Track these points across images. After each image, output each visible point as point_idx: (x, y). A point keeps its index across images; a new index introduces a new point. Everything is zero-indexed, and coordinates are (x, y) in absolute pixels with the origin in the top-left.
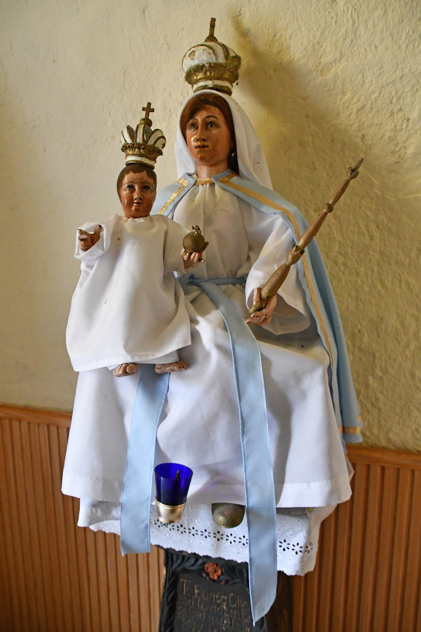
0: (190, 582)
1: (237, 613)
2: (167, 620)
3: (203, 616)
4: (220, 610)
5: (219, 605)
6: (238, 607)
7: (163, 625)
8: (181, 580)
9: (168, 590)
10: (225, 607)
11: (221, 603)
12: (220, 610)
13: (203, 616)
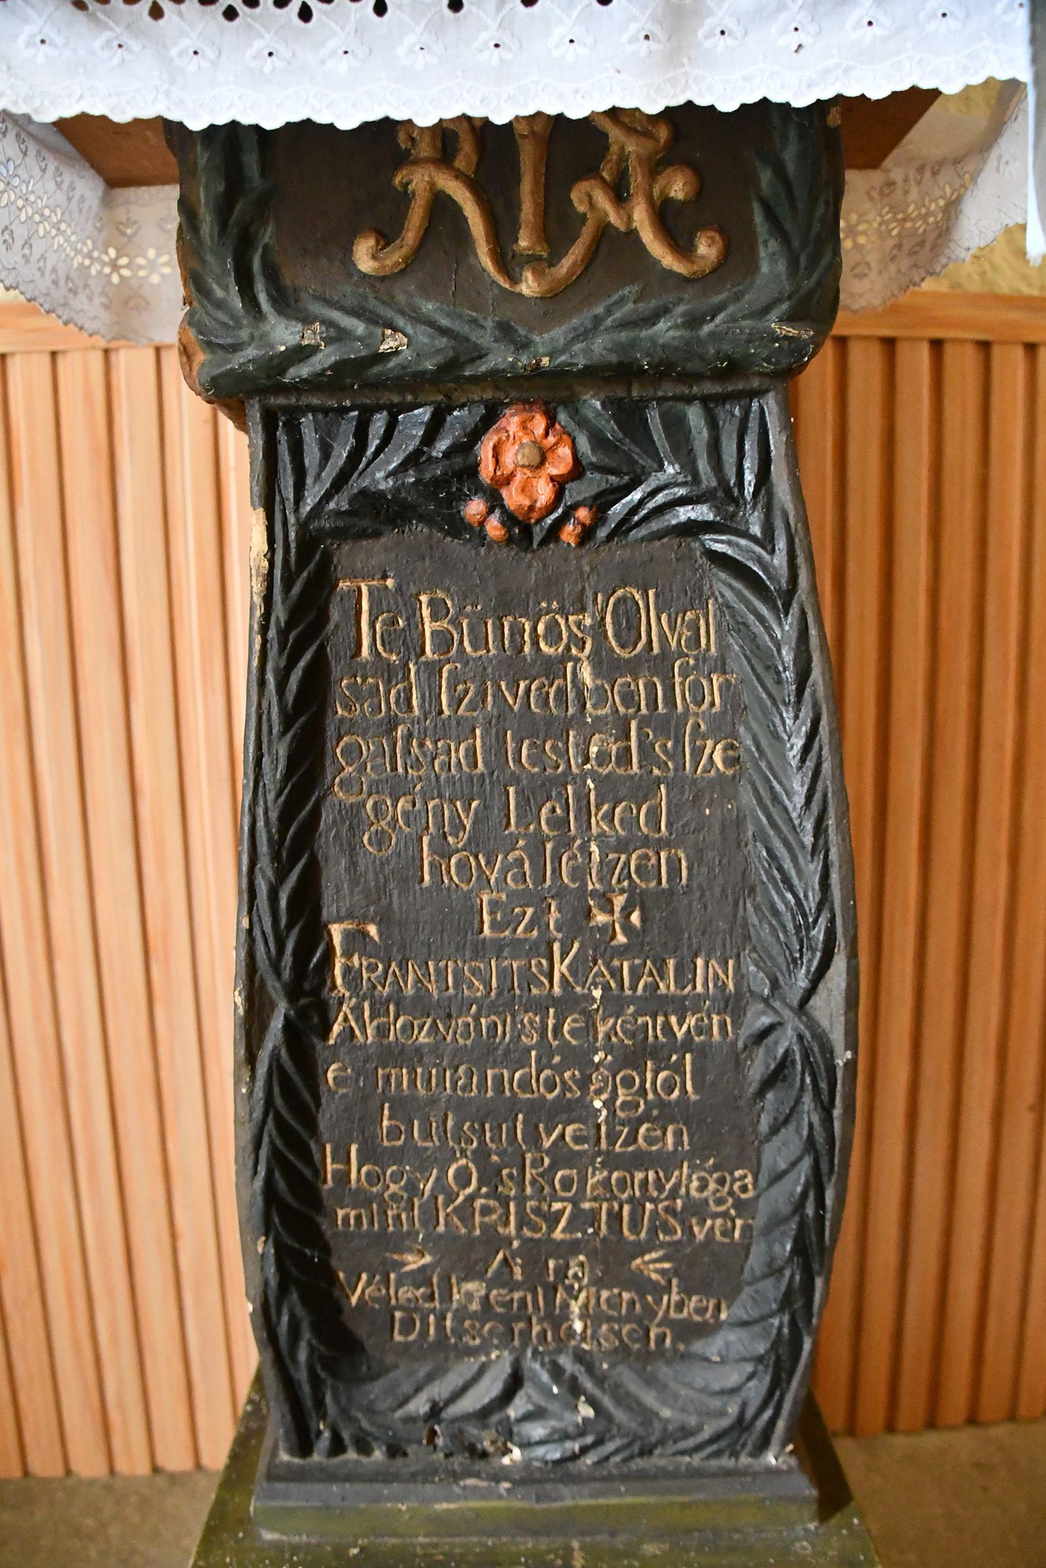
0: (390, 583)
1: (651, 688)
2: (286, 817)
3: (471, 753)
4: (561, 693)
5: (552, 668)
6: (656, 650)
7: (263, 848)
8: (344, 585)
9: (283, 634)
10: (586, 674)
11: (566, 656)
12: (561, 693)
13: (471, 753)
